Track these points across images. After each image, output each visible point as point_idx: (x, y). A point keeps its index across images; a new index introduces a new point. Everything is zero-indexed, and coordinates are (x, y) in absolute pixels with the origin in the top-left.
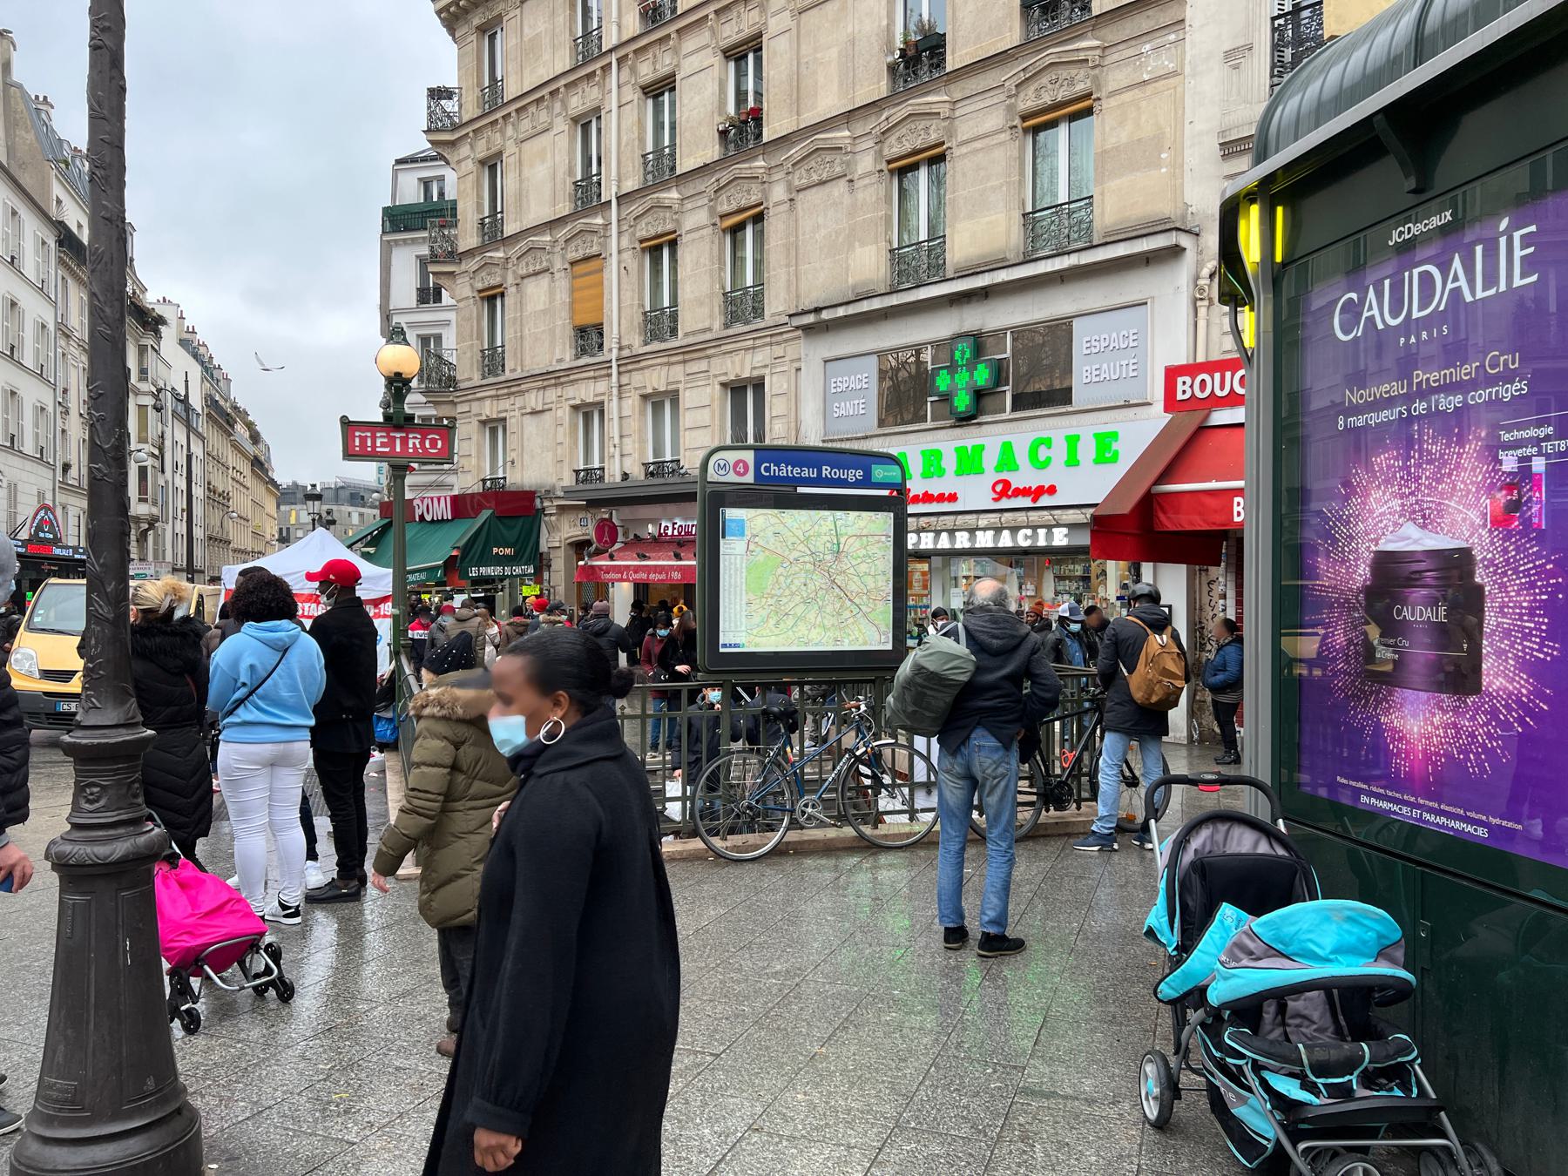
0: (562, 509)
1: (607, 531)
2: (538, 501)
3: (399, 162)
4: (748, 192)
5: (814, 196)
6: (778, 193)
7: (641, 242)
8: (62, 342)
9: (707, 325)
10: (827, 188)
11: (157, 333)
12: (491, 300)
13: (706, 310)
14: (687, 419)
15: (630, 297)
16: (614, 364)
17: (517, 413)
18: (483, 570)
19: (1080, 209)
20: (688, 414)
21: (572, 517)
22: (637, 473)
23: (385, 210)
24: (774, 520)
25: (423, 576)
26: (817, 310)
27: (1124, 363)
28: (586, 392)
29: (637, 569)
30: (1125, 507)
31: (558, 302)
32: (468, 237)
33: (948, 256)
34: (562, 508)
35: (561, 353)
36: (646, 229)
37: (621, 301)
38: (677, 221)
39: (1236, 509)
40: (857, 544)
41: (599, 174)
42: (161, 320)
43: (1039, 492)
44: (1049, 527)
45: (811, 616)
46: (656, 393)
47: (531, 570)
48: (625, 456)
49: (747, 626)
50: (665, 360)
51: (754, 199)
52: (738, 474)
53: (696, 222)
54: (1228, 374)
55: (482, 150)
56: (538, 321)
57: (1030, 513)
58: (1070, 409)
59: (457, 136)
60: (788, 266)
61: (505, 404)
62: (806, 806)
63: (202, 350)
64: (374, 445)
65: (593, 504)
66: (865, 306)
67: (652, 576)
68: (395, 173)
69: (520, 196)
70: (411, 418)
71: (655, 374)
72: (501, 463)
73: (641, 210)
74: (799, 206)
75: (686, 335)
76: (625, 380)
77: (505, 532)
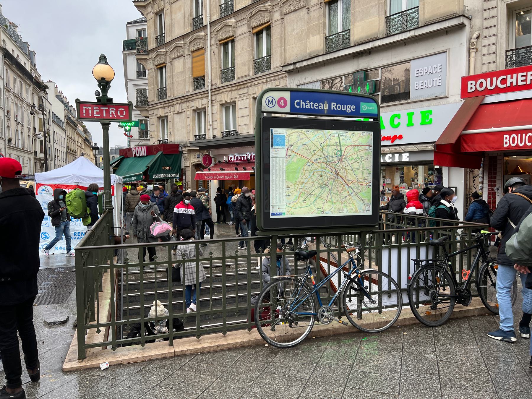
0: (190, 151)
1: (208, 160)
2: (180, 148)
3: (129, 23)
4: (264, 17)
5: (292, 16)
6: (277, 16)
7: (220, 41)
8: (7, 93)
9: (247, 73)
10: (297, 13)
11: (45, 91)
12: (161, 69)
13: (247, 68)
14: (239, 113)
15: (215, 64)
16: (209, 92)
17: (171, 114)
18: (159, 176)
19: (412, 13)
20: (240, 111)
21: (194, 154)
22: (219, 135)
23: (124, 42)
24: (302, 136)
25: (135, 178)
26: (294, 63)
27: (435, 79)
28: (198, 104)
29: (220, 175)
30: (453, 141)
31: (187, 68)
32: (152, 45)
33: (351, 38)
34: (190, 151)
35: (188, 88)
36: (222, 36)
37: (212, 66)
38: (234, 31)
39: (505, 141)
40: (352, 151)
41: (202, 15)
42: (46, 87)
43: (395, 138)
44: (400, 153)
45: (325, 195)
46: (226, 103)
47: (178, 175)
48: (214, 129)
49: (286, 202)
50: (230, 89)
51: (266, 19)
52: (281, 106)
53: (242, 31)
54: (495, 79)
55: (156, 8)
56: (179, 76)
57: (390, 148)
58: (409, 101)
59: (146, 3)
60: (281, 47)
61: (167, 110)
62: (323, 311)
63: (64, 99)
64: (93, 113)
65: (202, 148)
66: (315, 60)
67: (226, 177)
68: (127, 27)
69: (171, 26)
70: (111, 100)
71: (226, 95)
72: (166, 133)
73: (219, 28)
74: (286, 21)
75: (238, 78)
76: (214, 98)
77: (166, 160)
